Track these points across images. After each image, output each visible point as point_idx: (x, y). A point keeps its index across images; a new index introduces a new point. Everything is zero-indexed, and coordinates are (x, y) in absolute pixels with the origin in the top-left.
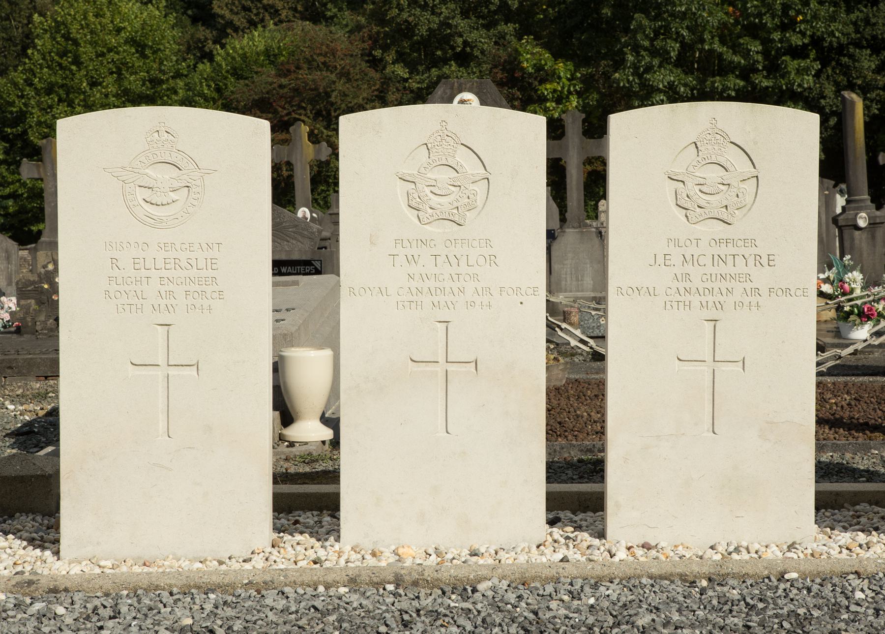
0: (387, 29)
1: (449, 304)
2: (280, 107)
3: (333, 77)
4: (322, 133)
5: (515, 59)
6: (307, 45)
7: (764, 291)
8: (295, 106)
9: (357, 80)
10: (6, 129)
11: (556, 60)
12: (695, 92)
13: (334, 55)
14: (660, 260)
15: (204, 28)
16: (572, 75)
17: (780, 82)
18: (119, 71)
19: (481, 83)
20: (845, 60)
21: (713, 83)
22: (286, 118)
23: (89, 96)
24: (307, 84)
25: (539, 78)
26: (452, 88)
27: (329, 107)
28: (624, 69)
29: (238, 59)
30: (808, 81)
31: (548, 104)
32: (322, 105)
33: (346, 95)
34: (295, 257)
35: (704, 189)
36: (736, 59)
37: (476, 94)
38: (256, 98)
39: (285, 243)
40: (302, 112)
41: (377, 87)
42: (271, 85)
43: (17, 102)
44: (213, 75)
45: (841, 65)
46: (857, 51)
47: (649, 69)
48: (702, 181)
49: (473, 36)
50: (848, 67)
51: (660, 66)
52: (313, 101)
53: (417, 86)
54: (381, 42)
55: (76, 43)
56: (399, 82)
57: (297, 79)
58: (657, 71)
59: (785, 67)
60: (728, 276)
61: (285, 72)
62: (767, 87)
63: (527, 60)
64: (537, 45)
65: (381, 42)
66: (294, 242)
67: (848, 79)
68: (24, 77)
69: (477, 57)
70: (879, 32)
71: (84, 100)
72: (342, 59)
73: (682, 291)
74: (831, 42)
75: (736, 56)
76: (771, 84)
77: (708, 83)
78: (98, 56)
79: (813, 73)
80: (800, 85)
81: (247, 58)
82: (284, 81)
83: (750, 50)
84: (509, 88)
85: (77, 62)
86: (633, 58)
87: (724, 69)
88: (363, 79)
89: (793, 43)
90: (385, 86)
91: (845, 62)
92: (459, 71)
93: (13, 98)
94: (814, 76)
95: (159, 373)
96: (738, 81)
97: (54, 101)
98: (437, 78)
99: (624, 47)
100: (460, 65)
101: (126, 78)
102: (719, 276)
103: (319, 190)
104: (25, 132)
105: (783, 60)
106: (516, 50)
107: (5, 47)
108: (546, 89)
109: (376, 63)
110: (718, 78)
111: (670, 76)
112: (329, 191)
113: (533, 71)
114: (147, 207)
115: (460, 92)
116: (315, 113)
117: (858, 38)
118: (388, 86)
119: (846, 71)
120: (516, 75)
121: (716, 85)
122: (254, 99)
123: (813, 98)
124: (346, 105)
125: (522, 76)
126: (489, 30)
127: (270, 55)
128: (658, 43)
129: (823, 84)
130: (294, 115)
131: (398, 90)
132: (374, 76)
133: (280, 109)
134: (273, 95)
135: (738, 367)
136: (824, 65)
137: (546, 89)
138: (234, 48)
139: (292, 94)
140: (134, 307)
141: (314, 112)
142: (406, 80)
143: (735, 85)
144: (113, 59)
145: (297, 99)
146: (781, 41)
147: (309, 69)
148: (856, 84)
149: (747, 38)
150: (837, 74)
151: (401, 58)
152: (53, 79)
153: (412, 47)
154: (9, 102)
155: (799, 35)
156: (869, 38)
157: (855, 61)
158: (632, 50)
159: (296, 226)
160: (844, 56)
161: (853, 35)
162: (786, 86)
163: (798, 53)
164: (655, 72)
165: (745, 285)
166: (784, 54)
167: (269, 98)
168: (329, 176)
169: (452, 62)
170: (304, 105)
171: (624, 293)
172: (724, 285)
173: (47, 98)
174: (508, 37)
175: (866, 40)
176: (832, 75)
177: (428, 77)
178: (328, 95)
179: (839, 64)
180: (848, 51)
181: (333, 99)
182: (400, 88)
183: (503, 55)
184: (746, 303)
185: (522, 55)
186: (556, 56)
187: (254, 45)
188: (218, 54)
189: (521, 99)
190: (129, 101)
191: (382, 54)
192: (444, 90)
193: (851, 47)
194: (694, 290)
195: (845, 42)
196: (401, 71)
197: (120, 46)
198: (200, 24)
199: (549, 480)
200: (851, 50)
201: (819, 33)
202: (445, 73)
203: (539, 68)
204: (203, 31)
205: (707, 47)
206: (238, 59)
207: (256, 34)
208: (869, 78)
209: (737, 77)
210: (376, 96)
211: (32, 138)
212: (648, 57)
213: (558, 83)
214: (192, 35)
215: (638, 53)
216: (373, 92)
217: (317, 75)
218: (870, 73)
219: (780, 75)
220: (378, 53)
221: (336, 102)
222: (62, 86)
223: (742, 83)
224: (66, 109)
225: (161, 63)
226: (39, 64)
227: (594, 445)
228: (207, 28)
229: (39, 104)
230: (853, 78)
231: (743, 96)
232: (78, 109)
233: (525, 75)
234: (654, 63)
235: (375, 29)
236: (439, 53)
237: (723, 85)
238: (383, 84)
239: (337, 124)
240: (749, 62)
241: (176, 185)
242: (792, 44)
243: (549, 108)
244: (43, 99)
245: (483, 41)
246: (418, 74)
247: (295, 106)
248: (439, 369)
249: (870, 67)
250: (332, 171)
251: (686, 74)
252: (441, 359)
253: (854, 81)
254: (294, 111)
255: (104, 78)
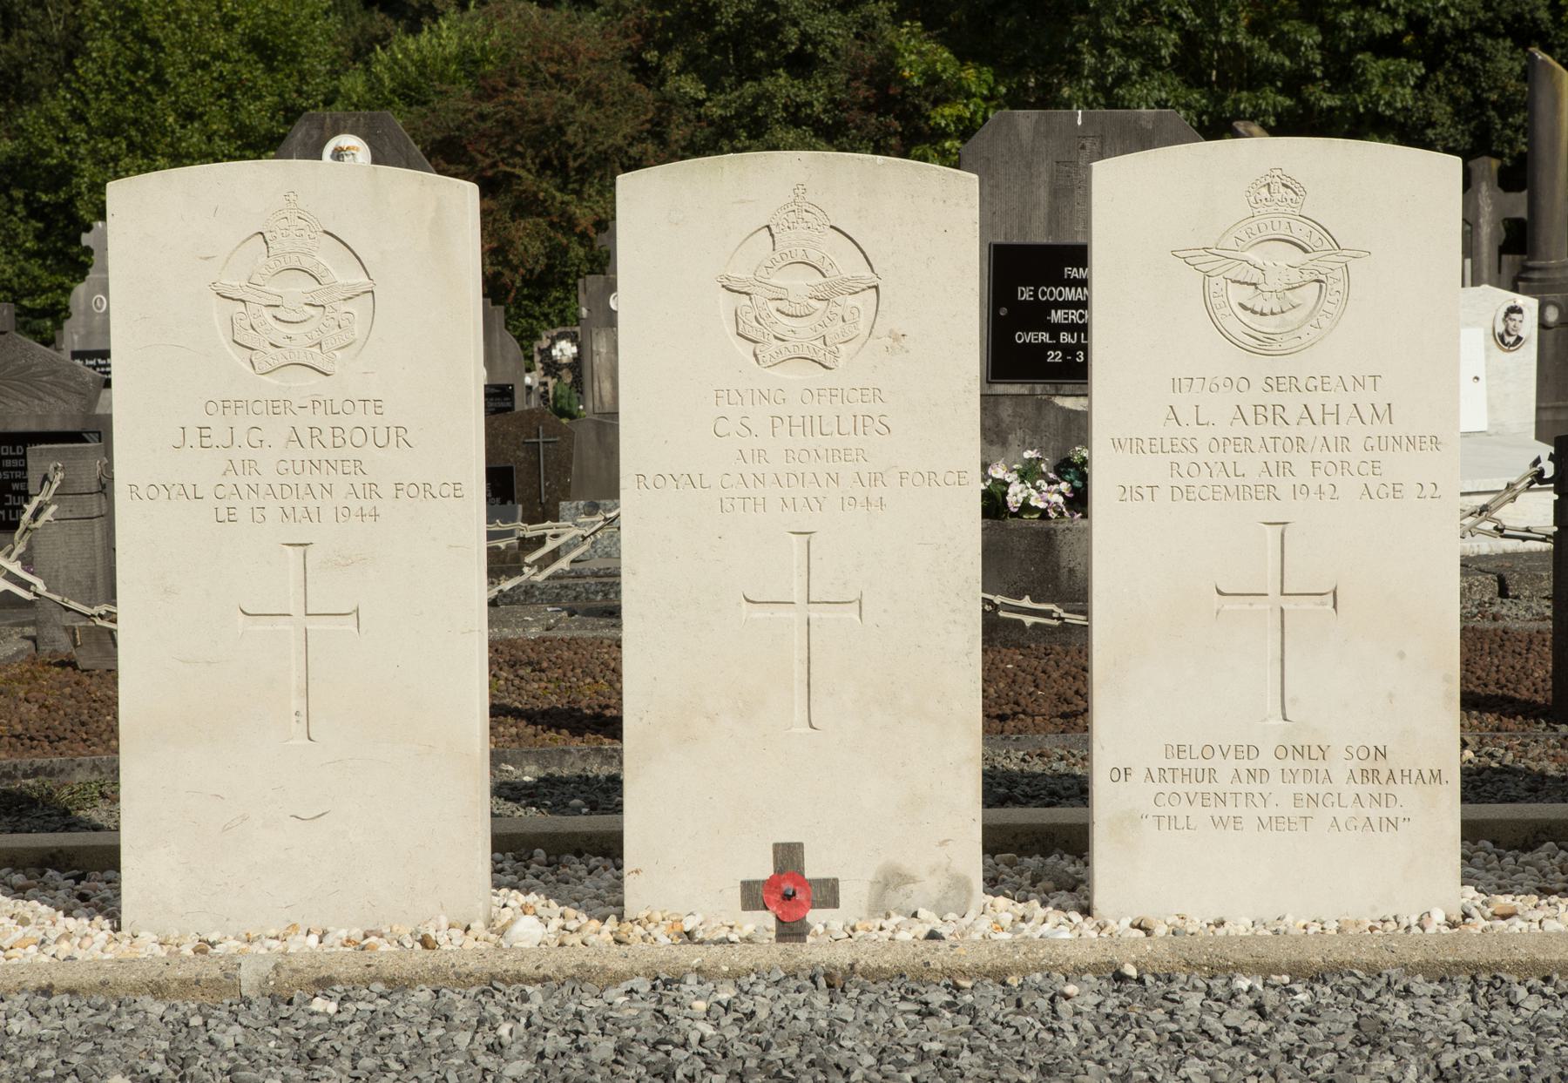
0: (668, 13)
1: (813, 502)
2: (480, 152)
3: (570, 99)
4: (554, 198)
5: (892, 64)
6: (526, 44)
7: (387, 490)
8: (505, 150)
9: (613, 104)
10: (38, 193)
11: (963, 64)
12: (1204, 118)
13: (574, 60)
14: (193, 437)
15: (382, 15)
16: (991, 90)
17: (1354, 100)
18: (228, 90)
19: (372, 118)
20: (1467, 58)
21: (1237, 102)
22: (490, 173)
23: (179, 139)
24: (526, 113)
25: (932, 98)
26: (322, 127)
27: (564, 151)
28: (1079, 80)
29: (412, 69)
30: (1405, 95)
31: (947, 144)
32: (552, 149)
33: (593, 130)
34: (54, 426)
35: (280, 313)
36: (1276, 58)
37: (365, 137)
38: (438, 137)
39: (36, 402)
40: (517, 160)
41: (650, 115)
42: (463, 115)
43: (56, 150)
44: (368, 97)
45: (1461, 67)
46: (1489, 41)
47: (1123, 78)
48: (1256, 276)
49: (817, 24)
50: (1473, 71)
51: (1143, 72)
52: (536, 143)
53: (719, 112)
54: (657, 36)
55: (155, 44)
56: (687, 106)
57: (510, 103)
58: (1136, 82)
59: (1363, 73)
60: (1405, 440)
61: (490, 91)
62: (1331, 109)
63: (910, 64)
64: (929, 37)
65: (657, 36)
66: (52, 400)
67: (1474, 91)
68: (69, 107)
69: (824, 60)
70: (1527, 8)
71: (171, 145)
72: (588, 68)
73: (750, 479)
74: (1441, 26)
75: (1276, 53)
76: (1339, 103)
77: (1228, 102)
78: (193, 70)
79: (1412, 83)
80: (1388, 105)
81: (426, 67)
82: (487, 107)
83: (1301, 43)
84: (880, 115)
85: (159, 80)
86: (1093, 60)
87: (1256, 78)
88: (625, 102)
89: (1377, 30)
90: (663, 115)
91: (1468, 62)
92: (793, 86)
93: (49, 142)
94: (1413, 88)
95: (795, 616)
96: (1280, 98)
97: (120, 148)
98: (754, 99)
99: (1079, 41)
100: (793, 75)
101: (242, 106)
102: (307, 464)
103: (551, 298)
104: (70, 201)
105: (1359, 60)
106: (892, 47)
107: (34, 55)
108: (943, 116)
109: (646, 73)
110: (1244, 94)
111: (1160, 90)
112: (568, 300)
113: (921, 83)
114: (1246, 317)
115: (336, 133)
116: (540, 163)
117: (1490, 20)
118: (670, 114)
119: (1470, 77)
120: (891, 92)
121: (1242, 106)
122: (434, 141)
123: (1414, 125)
124: (595, 148)
125: (902, 94)
126: (845, 13)
127: (468, 61)
128: (1139, 34)
129: (1429, 100)
130: (503, 168)
131: (687, 120)
132: (644, 95)
133: (479, 157)
134: (468, 132)
135: (851, 613)
136: (1431, 68)
137: (943, 116)
138: (405, 51)
139: (500, 130)
140: (750, 503)
141: (537, 161)
142: (700, 103)
143: (1275, 107)
144: (221, 72)
145: (508, 138)
146: (1355, 26)
147: (532, 85)
148: (1487, 99)
149: (1294, 22)
150: (1454, 83)
151: (692, 64)
152: (120, 110)
153: (714, 43)
154: (41, 149)
155: (1386, 16)
156: (1509, 18)
157: (1485, 59)
158: (1093, 44)
159: (54, 372)
160: (1466, 51)
161: (1481, 15)
162: (1365, 107)
163: (1386, 47)
164: (1133, 85)
165: (352, 478)
166: (1363, 50)
167: (460, 137)
168: (567, 274)
169: (781, 70)
170: (520, 148)
171: (1355, 471)
172: (316, 479)
173: (108, 142)
174: (880, 24)
175: (1504, 22)
176: (1445, 85)
177: (739, 97)
178: (561, 130)
179: (1457, 64)
180: (1473, 43)
181: (570, 137)
182: (691, 117)
183: (870, 56)
184: (1313, 489)
185: (903, 57)
186: (962, 57)
187: (440, 45)
188: (378, 61)
189: (901, 134)
190: (249, 146)
191: (660, 59)
192: (307, 133)
193: (1478, 35)
194: (263, 489)
195: (1467, 27)
196: (691, 87)
197: (233, 49)
198: (375, 9)
199: (987, 804)
200: (1478, 41)
201: (1421, 11)
202: (768, 90)
203: (932, 79)
204: (383, 21)
205: (1224, 39)
206: (412, 69)
207: (444, 25)
208: (1511, 90)
209: (1280, 91)
210: (649, 132)
211: (82, 213)
212: (1120, 56)
213: (966, 106)
214: (363, 28)
215: (1102, 51)
216: (642, 124)
217: (543, 96)
218: (1513, 81)
219: (1354, 87)
220: (651, 56)
221: (575, 144)
222: (135, 122)
223: (1288, 102)
224: (140, 162)
225: (302, 79)
226: (94, 84)
227: (15, 766)
228: (390, 16)
229: (94, 152)
230: (1483, 90)
231: (1286, 125)
232: (161, 161)
233: (908, 92)
234: (1131, 69)
235: (648, 13)
236: (760, 54)
237: (1255, 107)
238: (660, 110)
239: (614, 185)
240: (1299, 64)
241: (1295, 277)
242: (1374, 32)
243: (949, 150)
244: (100, 145)
245: (835, 31)
246: (723, 91)
247: (505, 150)
248: (795, 616)
249: (1511, 70)
250: (573, 265)
251: (1190, 87)
252: (1273, 588)
253: (1485, 95)
254: (503, 160)
255: (205, 106)
